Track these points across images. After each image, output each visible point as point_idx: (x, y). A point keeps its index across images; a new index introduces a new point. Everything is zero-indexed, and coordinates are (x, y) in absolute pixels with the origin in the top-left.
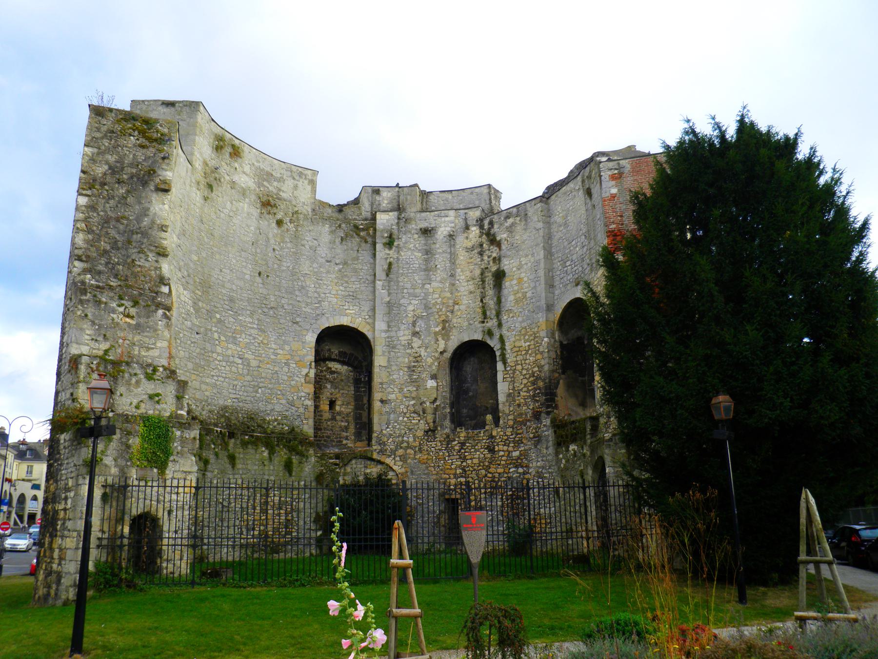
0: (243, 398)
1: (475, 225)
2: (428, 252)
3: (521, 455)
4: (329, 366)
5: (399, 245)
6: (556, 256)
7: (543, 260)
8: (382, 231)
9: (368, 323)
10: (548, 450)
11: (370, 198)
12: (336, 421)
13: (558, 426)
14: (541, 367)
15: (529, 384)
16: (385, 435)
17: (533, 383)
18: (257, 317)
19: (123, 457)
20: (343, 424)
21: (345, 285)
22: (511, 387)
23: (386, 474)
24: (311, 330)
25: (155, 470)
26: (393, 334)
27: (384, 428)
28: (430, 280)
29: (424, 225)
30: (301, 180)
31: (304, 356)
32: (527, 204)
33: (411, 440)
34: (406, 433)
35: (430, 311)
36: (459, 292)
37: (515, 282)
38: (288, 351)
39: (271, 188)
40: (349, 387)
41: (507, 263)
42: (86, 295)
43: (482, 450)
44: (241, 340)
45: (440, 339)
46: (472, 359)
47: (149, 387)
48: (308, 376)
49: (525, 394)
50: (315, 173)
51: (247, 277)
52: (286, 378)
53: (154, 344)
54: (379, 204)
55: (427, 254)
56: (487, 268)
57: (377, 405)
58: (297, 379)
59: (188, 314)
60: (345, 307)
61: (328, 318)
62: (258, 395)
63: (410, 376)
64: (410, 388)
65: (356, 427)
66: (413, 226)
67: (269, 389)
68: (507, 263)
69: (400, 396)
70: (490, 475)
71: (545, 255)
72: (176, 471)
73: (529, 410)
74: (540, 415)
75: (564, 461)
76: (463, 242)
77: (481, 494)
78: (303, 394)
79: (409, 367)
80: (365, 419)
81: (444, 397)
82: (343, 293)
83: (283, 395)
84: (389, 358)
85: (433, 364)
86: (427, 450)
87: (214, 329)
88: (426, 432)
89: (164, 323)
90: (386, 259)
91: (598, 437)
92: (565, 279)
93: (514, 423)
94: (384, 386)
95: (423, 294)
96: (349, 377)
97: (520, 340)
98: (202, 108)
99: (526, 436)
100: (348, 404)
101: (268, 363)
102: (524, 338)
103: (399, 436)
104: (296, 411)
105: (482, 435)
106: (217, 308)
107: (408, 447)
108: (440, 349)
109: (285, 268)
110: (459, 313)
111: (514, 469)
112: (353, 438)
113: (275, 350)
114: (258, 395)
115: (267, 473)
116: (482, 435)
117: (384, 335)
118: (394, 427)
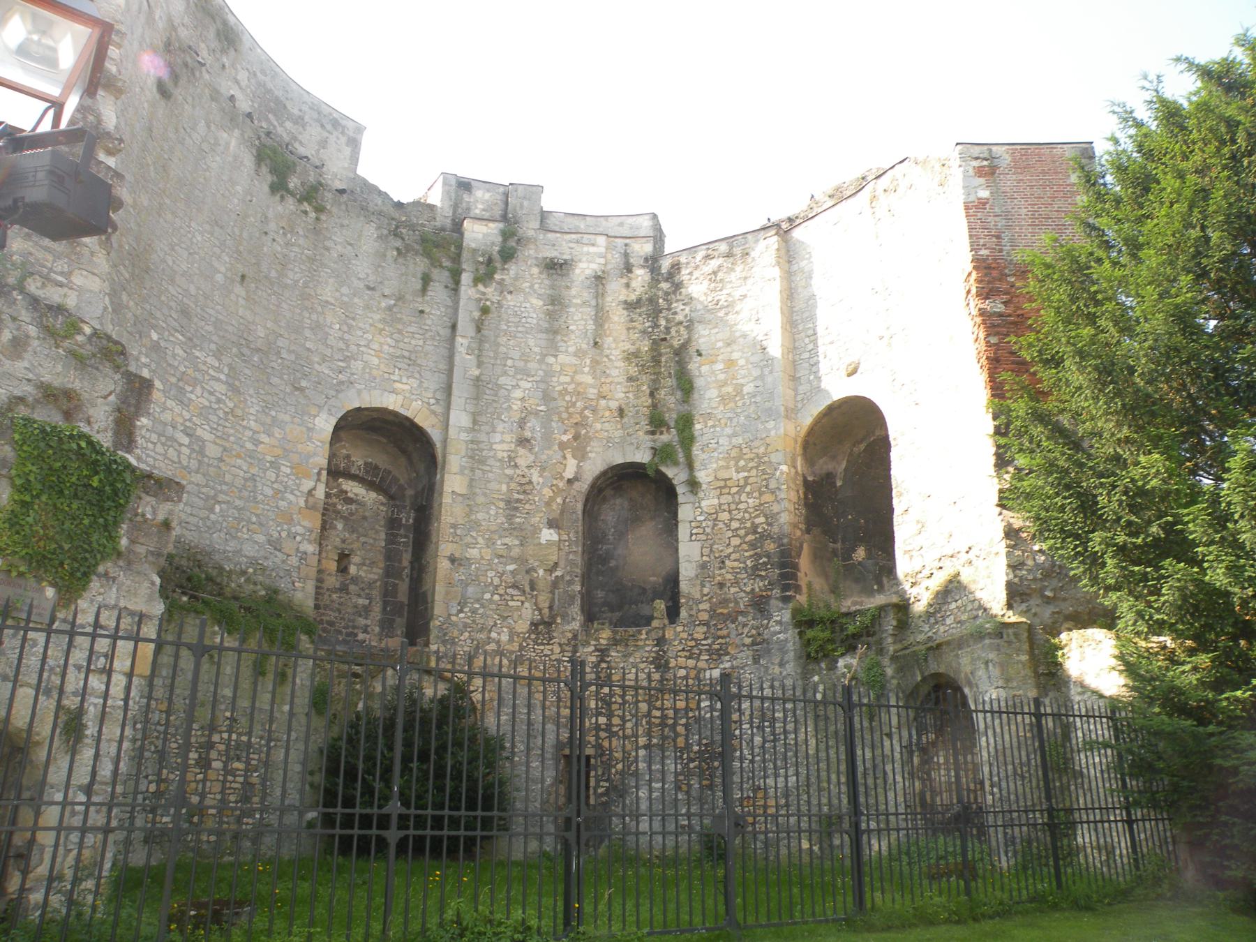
1: (643, 267)
2: (556, 303)
4: (344, 487)
6: (801, 327)
8: (475, 251)
9: (434, 413)
11: (453, 195)
12: (348, 593)
13: (804, 622)
15: (745, 547)
16: (454, 625)
17: (753, 545)
18: (226, 360)
21: (395, 336)
22: (706, 551)
25: (50, 592)
27: (454, 611)
28: (557, 349)
29: (550, 253)
30: (335, 133)
31: (309, 456)
32: (749, 236)
33: (505, 638)
34: (495, 624)
35: (552, 405)
37: (720, 366)
39: (280, 130)
40: (377, 532)
44: (193, 397)
45: (569, 456)
46: (618, 501)
49: (736, 564)
50: (360, 129)
52: (269, 492)
53: (68, 275)
55: (553, 304)
56: (665, 339)
57: (443, 565)
58: (291, 497)
60: (392, 377)
61: (359, 392)
63: (510, 518)
64: (507, 540)
66: (531, 252)
67: (236, 508)
68: (703, 332)
72: (106, 607)
73: (743, 594)
74: (767, 603)
75: (821, 688)
76: (616, 292)
77: (637, 749)
78: (299, 529)
79: (508, 502)
81: (571, 563)
82: (391, 350)
83: (261, 524)
84: (472, 480)
85: (552, 499)
87: (143, 360)
91: (906, 643)
93: (711, 617)
94: (459, 532)
95: (541, 373)
96: (378, 515)
97: (728, 467)
99: (737, 641)
100: (373, 564)
101: (238, 456)
102: (736, 464)
103: (481, 630)
104: (284, 562)
105: (644, 636)
106: (155, 318)
108: (569, 474)
109: (289, 282)
112: (377, 629)
113: (255, 432)
114: (212, 516)
116: (644, 636)
117: (464, 436)
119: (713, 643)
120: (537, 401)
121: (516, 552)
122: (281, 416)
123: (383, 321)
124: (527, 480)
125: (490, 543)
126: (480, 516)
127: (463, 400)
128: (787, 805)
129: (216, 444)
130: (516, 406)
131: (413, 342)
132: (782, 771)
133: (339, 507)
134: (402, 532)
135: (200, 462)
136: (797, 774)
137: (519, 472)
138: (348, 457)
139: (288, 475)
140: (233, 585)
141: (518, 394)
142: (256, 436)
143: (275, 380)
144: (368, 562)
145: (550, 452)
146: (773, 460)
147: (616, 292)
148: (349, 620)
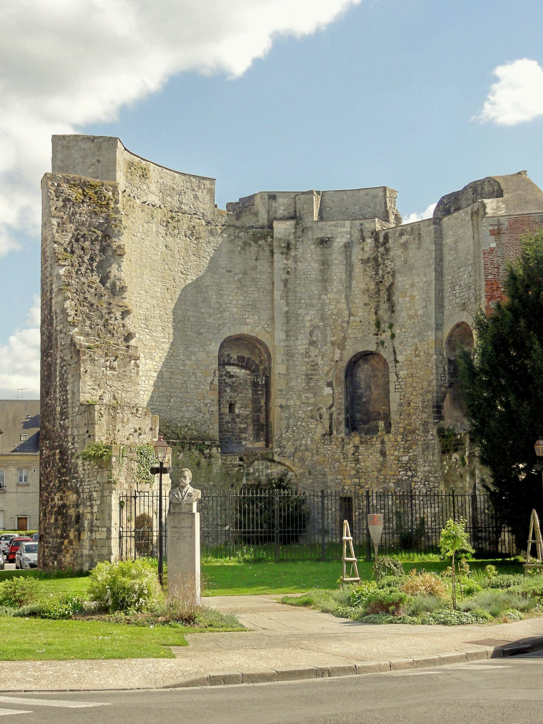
0: (159, 408)
2: (325, 264)
3: (410, 459)
4: (229, 370)
5: (296, 255)
7: (434, 281)
8: (280, 240)
9: (267, 332)
10: (434, 456)
11: (267, 205)
14: (430, 382)
20: (242, 426)
23: (285, 475)
24: (214, 340)
28: (327, 290)
33: (309, 442)
34: (304, 437)
36: (355, 303)
37: (407, 299)
40: (247, 390)
41: (401, 279)
43: (374, 454)
44: (155, 354)
46: (366, 366)
48: (213, 384)
51: (159, 294)
52: (193, 386)
54: (276, 211)
55: (323, 265)
56: (381, 282)
58: (203, 387)
60: (245, 316)
61: (229, 328)
62: (171, 404)
63: (308, 383)
64: (307, 395)
65: (254, 428)
69: (298, 403)
70: (382, 477)
71: (436, 277)
75: (447, 467)
78: (209, 401)
79: (307, 375)
80: (263, 421)
81: (340, 404)
84: (288, 366)
86: (324, 453)
88: (324, 435)
90: (285, 269)
92: (454, 301)
93: (404, 430)
95: (319, 305)
96: (247, 381)
98: (119, 143)
101: (178, 374)
104: (203, 417)
105: (375, 440)
107: (307, 450)
110: (354, 324)
111: (403, 472)
113: (183, 361)
116: (375, 440)
117: (282, 344)
118: (293, 431)
119: (405, 443)
120: (318, 321)
121: (312, 401)
122: (194, 349)
125: (299, 397)
126: (294, 384)
128: (435, 521)
130: (308, 324)
131: (253, 296)
132: (433, 505)
133: (227, 381)
134: (259, 388)
135: (162, 382)
136: (438, 507)
137: (311, 359)
138: (228, 355)
139: (200, 377)
140: (183, 432)
141: (308, 318)
142: (184, 363)
143: (189, 333)
145: (326, 348)
146: (430, 352)
147: (357, 255)
148: (238, 436)
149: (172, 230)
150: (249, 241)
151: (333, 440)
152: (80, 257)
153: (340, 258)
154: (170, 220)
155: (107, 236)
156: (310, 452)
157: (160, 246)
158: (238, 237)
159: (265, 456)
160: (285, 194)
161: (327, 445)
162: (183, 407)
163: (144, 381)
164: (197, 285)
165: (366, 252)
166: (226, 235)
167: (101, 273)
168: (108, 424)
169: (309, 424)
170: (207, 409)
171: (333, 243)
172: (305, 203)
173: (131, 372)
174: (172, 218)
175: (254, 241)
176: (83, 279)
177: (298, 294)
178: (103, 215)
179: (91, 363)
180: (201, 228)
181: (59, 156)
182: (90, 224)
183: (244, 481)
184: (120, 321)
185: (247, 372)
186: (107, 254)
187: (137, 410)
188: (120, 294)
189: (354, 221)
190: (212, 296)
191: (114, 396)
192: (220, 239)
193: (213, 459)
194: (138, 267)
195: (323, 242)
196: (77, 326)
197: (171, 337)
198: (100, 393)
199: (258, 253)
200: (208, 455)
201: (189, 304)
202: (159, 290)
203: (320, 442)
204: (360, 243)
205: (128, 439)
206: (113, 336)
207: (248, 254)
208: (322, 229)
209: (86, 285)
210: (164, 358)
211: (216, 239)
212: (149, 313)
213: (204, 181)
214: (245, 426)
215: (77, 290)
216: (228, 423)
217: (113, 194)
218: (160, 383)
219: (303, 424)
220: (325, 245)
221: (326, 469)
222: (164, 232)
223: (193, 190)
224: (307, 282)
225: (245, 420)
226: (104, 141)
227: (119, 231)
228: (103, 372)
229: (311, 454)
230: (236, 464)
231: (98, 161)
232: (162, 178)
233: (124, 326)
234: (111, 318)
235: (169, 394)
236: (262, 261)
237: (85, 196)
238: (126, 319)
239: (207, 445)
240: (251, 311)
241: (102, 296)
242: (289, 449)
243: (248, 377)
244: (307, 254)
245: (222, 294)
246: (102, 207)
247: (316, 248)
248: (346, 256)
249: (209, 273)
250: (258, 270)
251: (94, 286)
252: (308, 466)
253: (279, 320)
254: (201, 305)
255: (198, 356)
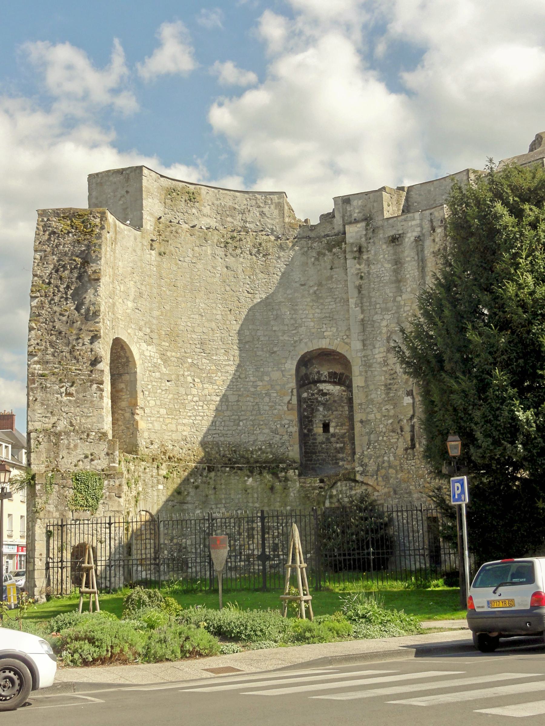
1: (440, 226)
2: (398, 263)
4: (321, 388)
5: (368, 258)
8: (352, 244)
11: (341, 210)
19: (62, 504)
20: (338, 445)
24: (290, 357)
26: (369, 352)
29: (392, 233)
33: (392, 458)
34: (386, 453)
38: (267, 381)
40: (343, 407)
42: (35, 384)
44: (217, 378)
47: (84, 449)
48: (291, 403)
52: (267, 408)
55: (396, 264)
58: (280, 407)
59: (155, 366)
61: (306, 343)
62: (239, 428)
63: (387, 394)
64: (387, 407)
72: (105, 511)
78: (287, 422)
79: (386, 385)
82: (319, 315)
84: (366, 377)
86: (408, 469)
87: (186, 373)
88: (406, 449)
89: (98, 394)
90: (358, 274)
96: (342, 397)
100: (342, 425)
101: (248, 396)
104: (281, 439)
107: (390, 467)
113: (253, 382)
115: (251, 500)
118: (375, 447)
121: (392, 413)
122: (266, 369)
123: (313, 301)
124: (394, 371)
125: (380, 410)
126: (373, 396)
127: (357, 334)
129: (234, 394)
130: (384, 330)
131: (330, 307)
133: (320, 399)
135: (227, 406)
137: (389, 368)
139: (275, 397)
141: (384, 323)
142: (255, 384)
144: (340, 424)
148: (333, 456)
149: (233, 250)
150: (323, 251)
151: (416, 454)
152: (57, 287)
153: (412, 254)
154: (229, 241)
155: (86, 262)
156: (394, 469)
157: (219, 268)
158: (311, 247)
159: (347, 476)
160: (359, 195)
161: (410, 460)
162: (256, 430)
163: (202, 406)
164: (267, 303)
165: (437, 243)
166: (297, 248)
167: (77, 300)
168: (48, 451)
169: (391, 438)
170: (285, 430)
171: (405, 239)
172: (374, 201)
173: (92, 396)
174: (233, 238)
175: (328, 250)
176: (56, 308)
177: (373, 300)
178: (86, 242)
179: (42, 391)
180: (269, 245)
181: (94, 194)
182: (72, 252)
183: (327, 504)
184: (88, 346)
185: (343, 388)
186: (83, 281)
187: (88, 435)
188: (93, 318)
189: (423, 212)
190: (285, 312)
191: (71, 422)
192: (292, 253)
193: (289, 482)
194: (187, 291)
195: (395, 239)
196: (36, 355)
197: (237, 359)
198: (54, 419)
199: (333, 262)
200: (284, 479)
201: (258, 324)
202: (219, 312)
203: (403, 457)
204: (431, 235)
205: (75, 466)
206: (78, 362)
207: (322, 264)
208: (393, 226)
209: (58, 314)
210: (229, 381)
211: (287, 254)
212: (205, 337)
213: (271, 196)
214: (342, 445)
215: (46, 320)
216: (323, 443)
217: (101, 220)
218: (224, 408)
219: (385, 438)
220: (397, 243)
221: (411, 487)
222: (224, 253)
223: (259, 207)
224: (381, 285)
225: (341, 439)
226: (131, 172)
227: (97, 256)
228: (57, 399)
229: (394, 471)
230: (316, 486)
231: (127, 192)
232: (217, 199)
233: (92, 350)
234: (79, 343)
235: (237, 417)
236: (337, 270)
237: (72, 226)
238: (96, 343)
239: (282, 468)
240: (329, 324)
241: (73, 323)
242: (372, 467)
243: (344, 393)
244: (380, 255)
245: (296, 309)
246: (86, 235)
247: (387, 247)
248: (417, 250)
249: (280, 290)
250: (334, 280)
251: (67, 314)
252: (393, 485)
253: (356, 329)
254: (272, 323)
255: (271, 375)
